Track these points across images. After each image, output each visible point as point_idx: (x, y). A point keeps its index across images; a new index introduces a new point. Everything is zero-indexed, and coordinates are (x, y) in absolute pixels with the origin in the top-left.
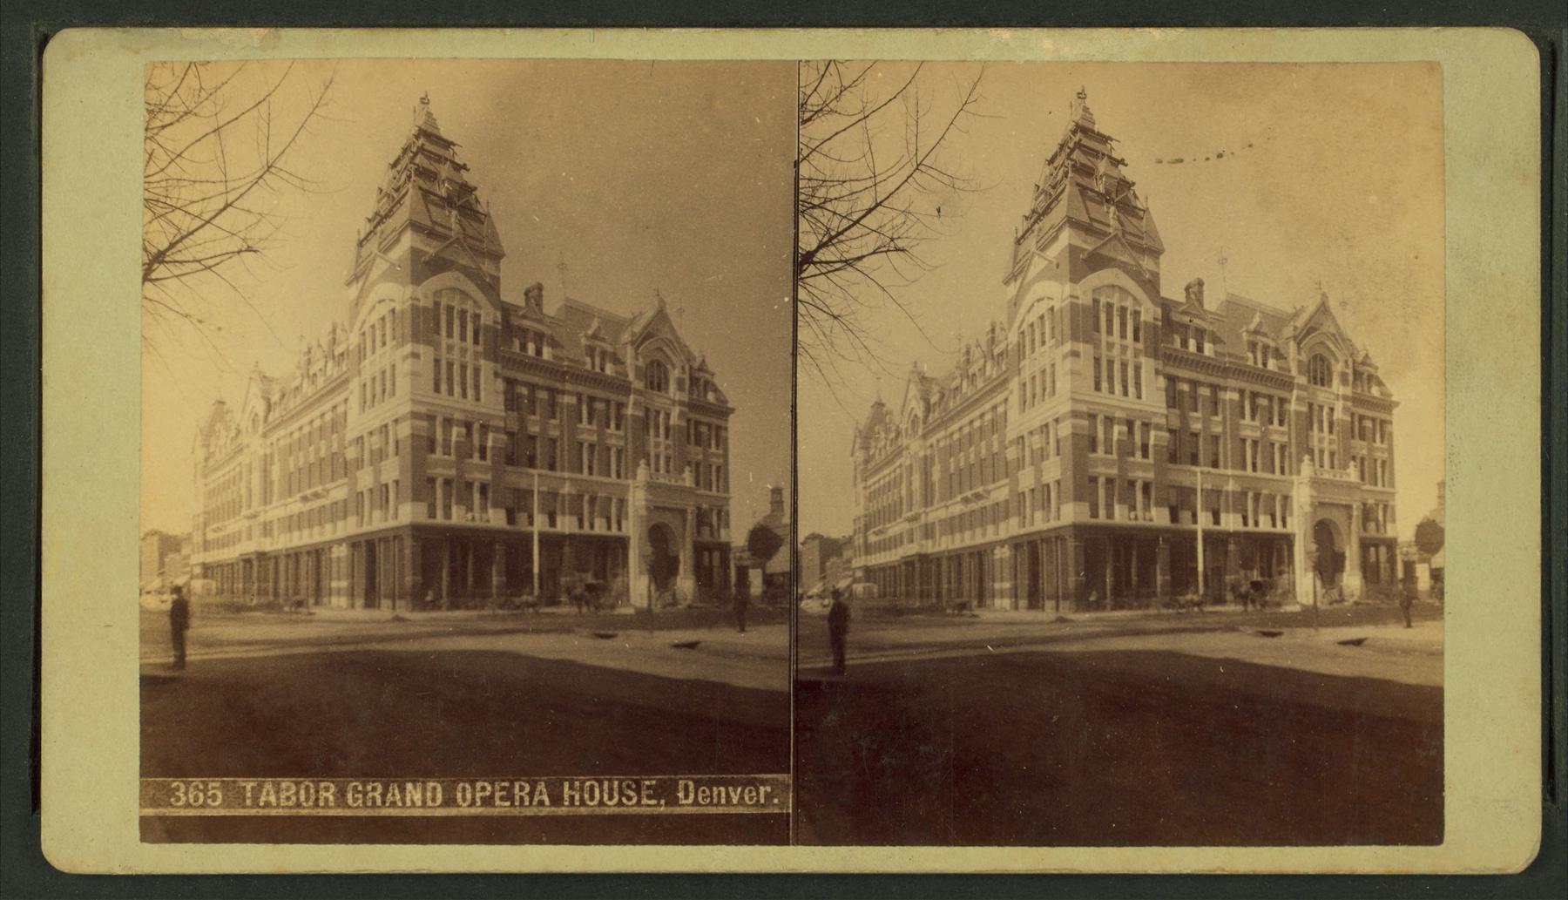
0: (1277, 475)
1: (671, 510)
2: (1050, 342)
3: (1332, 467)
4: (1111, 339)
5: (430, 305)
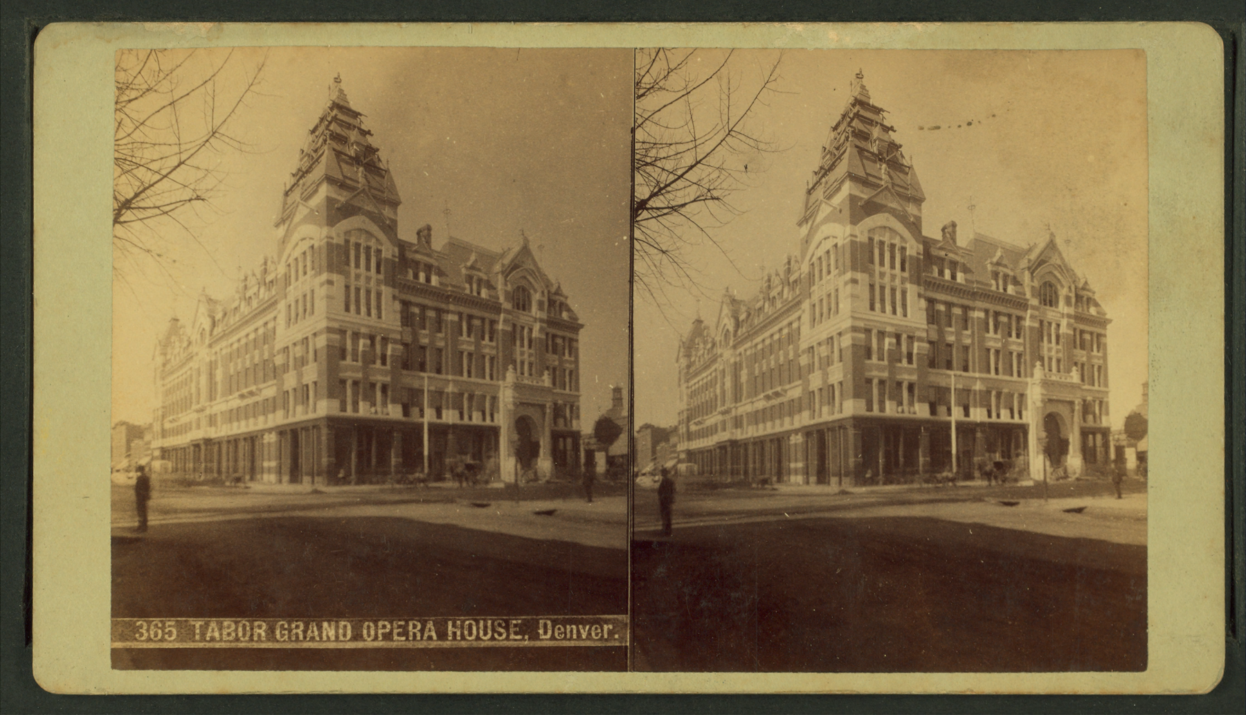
5: (342, 243)
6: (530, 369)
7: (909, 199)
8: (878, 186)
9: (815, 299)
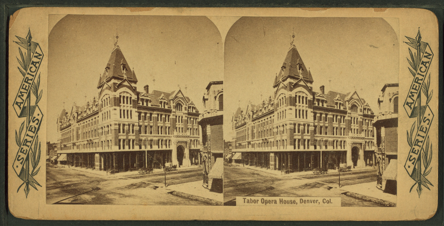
0: (167, 135)
1: (183, 142)
2: (285, 105)
3: (182, 132)
4: (300, 104)
6: (308, 143)
7: (308, 82)
8: (123, 79)
9: (103, 112)
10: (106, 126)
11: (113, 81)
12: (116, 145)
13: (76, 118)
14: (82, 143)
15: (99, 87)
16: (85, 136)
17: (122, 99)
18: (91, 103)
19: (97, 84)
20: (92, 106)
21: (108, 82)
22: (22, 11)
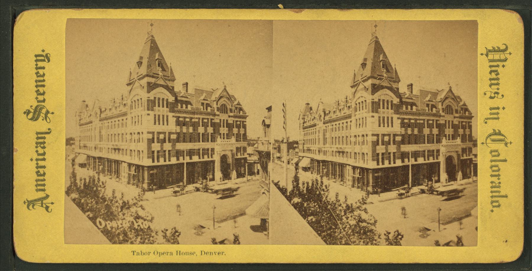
9: (133, 115)
10: (361, 135)
11: (146, 80)
12: (148, 157)
13: (322, 118)
14: (331, 150)
15: (128, 85)
16: (334, 142)
17: (381, 103)
18: (118, 101)
19: (350, 83)
20: (119, 105)
21: (364, 81)
22: (26, 13)
